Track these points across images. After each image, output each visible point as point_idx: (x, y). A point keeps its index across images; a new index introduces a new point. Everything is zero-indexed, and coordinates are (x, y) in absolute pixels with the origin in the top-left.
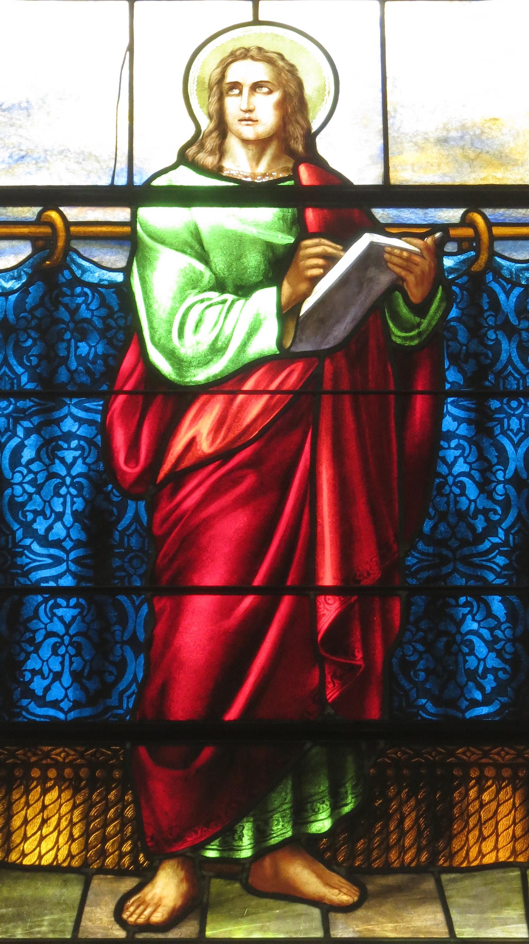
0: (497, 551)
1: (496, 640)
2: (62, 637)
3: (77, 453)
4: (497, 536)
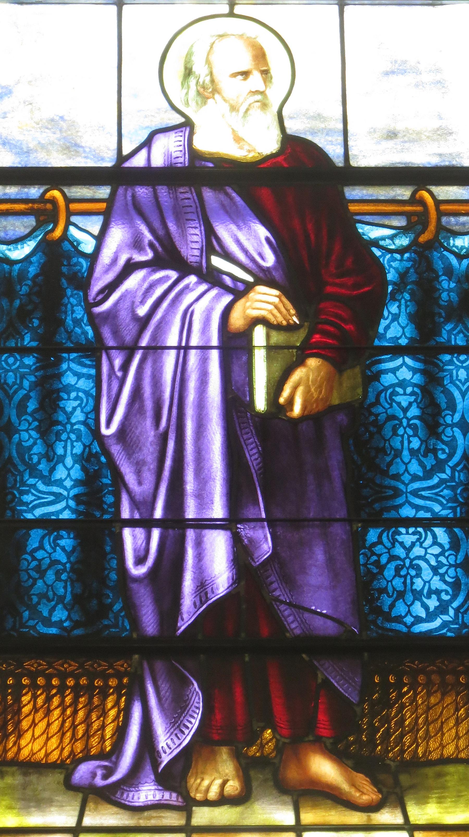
0: (444, 485)
1: (440, 565)
2: (403, 560)
3: (412, 399)
4: (448, 614)
